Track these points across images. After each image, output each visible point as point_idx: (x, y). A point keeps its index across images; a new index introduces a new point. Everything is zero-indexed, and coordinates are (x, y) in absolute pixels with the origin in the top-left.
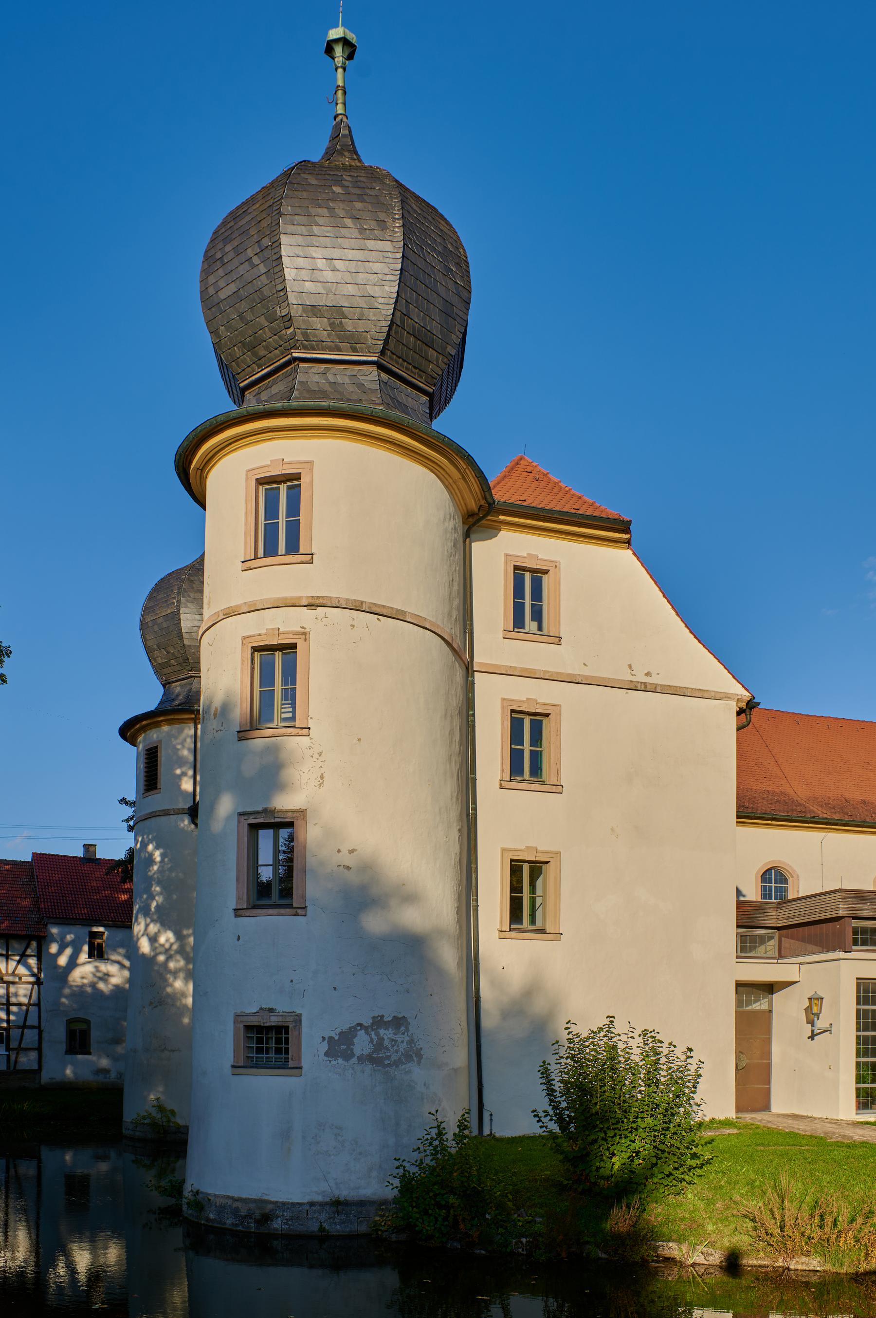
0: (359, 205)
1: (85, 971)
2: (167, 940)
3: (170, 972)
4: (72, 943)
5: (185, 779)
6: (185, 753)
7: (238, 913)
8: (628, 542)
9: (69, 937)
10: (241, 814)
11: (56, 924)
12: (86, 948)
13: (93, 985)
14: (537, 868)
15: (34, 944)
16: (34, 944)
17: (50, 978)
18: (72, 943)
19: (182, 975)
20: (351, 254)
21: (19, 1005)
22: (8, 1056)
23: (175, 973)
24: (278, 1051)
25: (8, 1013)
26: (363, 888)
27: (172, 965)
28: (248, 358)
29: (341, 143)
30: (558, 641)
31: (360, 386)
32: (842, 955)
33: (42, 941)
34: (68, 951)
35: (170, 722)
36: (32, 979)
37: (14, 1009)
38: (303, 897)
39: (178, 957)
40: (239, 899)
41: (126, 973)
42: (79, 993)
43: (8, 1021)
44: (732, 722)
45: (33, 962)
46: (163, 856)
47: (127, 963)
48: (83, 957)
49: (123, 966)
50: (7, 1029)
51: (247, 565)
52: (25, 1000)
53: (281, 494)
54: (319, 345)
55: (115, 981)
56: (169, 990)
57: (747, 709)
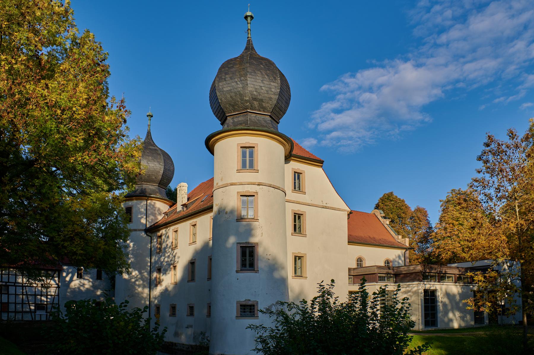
0: (268, 72)
1: (76, 283)
2: (136, 274)
3: (137, 285)
4: (71, 272)
5: (143, 219)
6: (143, 210)
7: (237, 272)
8: (322, 166)
9: (70, 270)
10: (237, 243)
11: (66, 265)
12: (76, 274)
13: (79, 288)
14: (300, 258)
15: (57, 273)
16: (57, 273)
17: (63, 286)
18: (71, 272)
19: (142, 286)
20: (267, 86)
21: (51, 295)
22: (47, 315)
23: (139, 286)
24: (250, 312)
25: (47, 298)
26: (274, 265)
27: (137, 283)
28: (231, 108)
29: (249, 47)
30: (305, 193)
31: (265, 121)
32: (376, 284)
33: (60, 271)
34: (70, 275)
35: (136, 199)
36: (56, 286)
37: (49, 297)
38: (258, 268)
39: (140, 280)
40: (237, 268)
41: (91, 284)
42: (74, 291)
43: (47, 301)
44: (346, 217)
45: (56, 279)
46: (133, 245)
47: (91, 280)
48: (75, 278)
49: (90, 281)
50: (46, 305)
51: (238, 171)
52: (53, 294)
53: (248, 151)
54: (255, 110)
55: (87, 286)
56: (136, 291)
57: (350, 214)
